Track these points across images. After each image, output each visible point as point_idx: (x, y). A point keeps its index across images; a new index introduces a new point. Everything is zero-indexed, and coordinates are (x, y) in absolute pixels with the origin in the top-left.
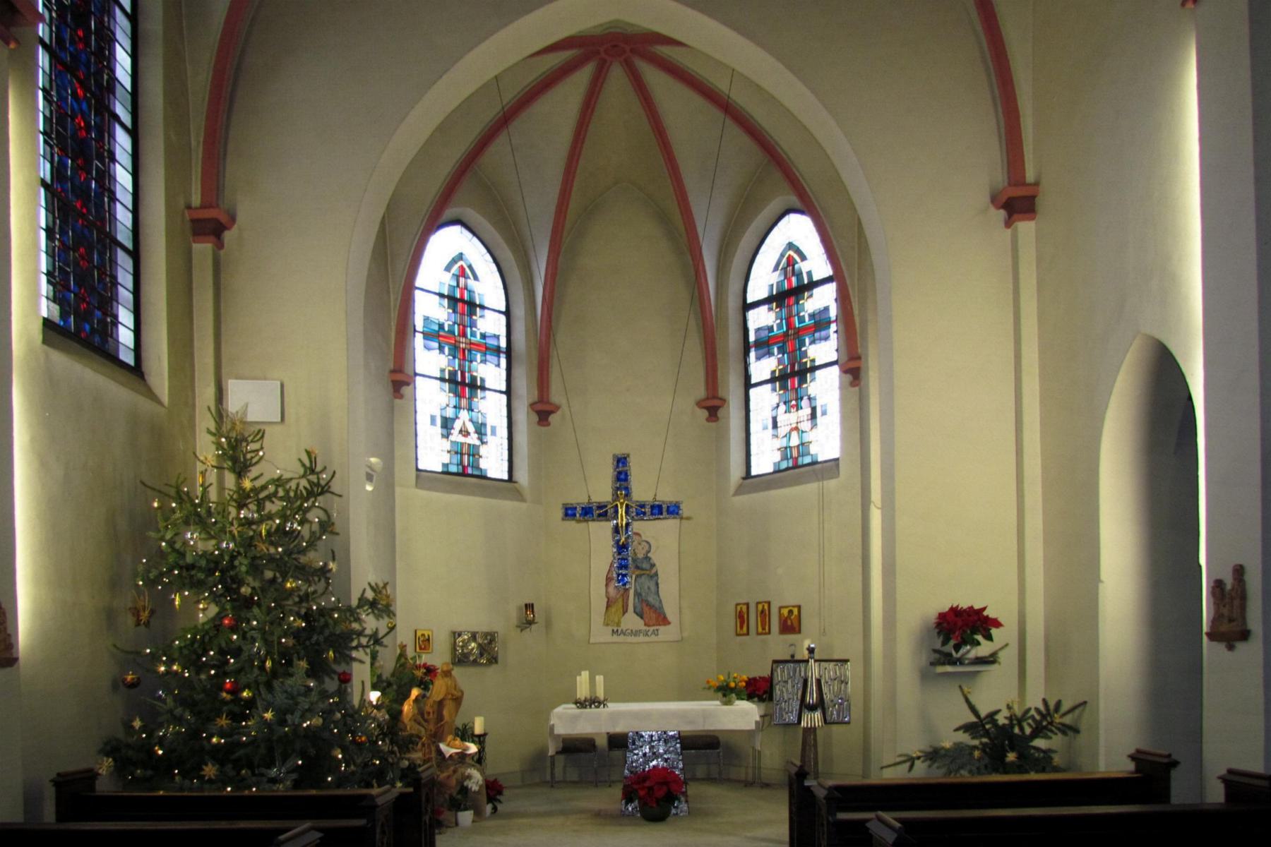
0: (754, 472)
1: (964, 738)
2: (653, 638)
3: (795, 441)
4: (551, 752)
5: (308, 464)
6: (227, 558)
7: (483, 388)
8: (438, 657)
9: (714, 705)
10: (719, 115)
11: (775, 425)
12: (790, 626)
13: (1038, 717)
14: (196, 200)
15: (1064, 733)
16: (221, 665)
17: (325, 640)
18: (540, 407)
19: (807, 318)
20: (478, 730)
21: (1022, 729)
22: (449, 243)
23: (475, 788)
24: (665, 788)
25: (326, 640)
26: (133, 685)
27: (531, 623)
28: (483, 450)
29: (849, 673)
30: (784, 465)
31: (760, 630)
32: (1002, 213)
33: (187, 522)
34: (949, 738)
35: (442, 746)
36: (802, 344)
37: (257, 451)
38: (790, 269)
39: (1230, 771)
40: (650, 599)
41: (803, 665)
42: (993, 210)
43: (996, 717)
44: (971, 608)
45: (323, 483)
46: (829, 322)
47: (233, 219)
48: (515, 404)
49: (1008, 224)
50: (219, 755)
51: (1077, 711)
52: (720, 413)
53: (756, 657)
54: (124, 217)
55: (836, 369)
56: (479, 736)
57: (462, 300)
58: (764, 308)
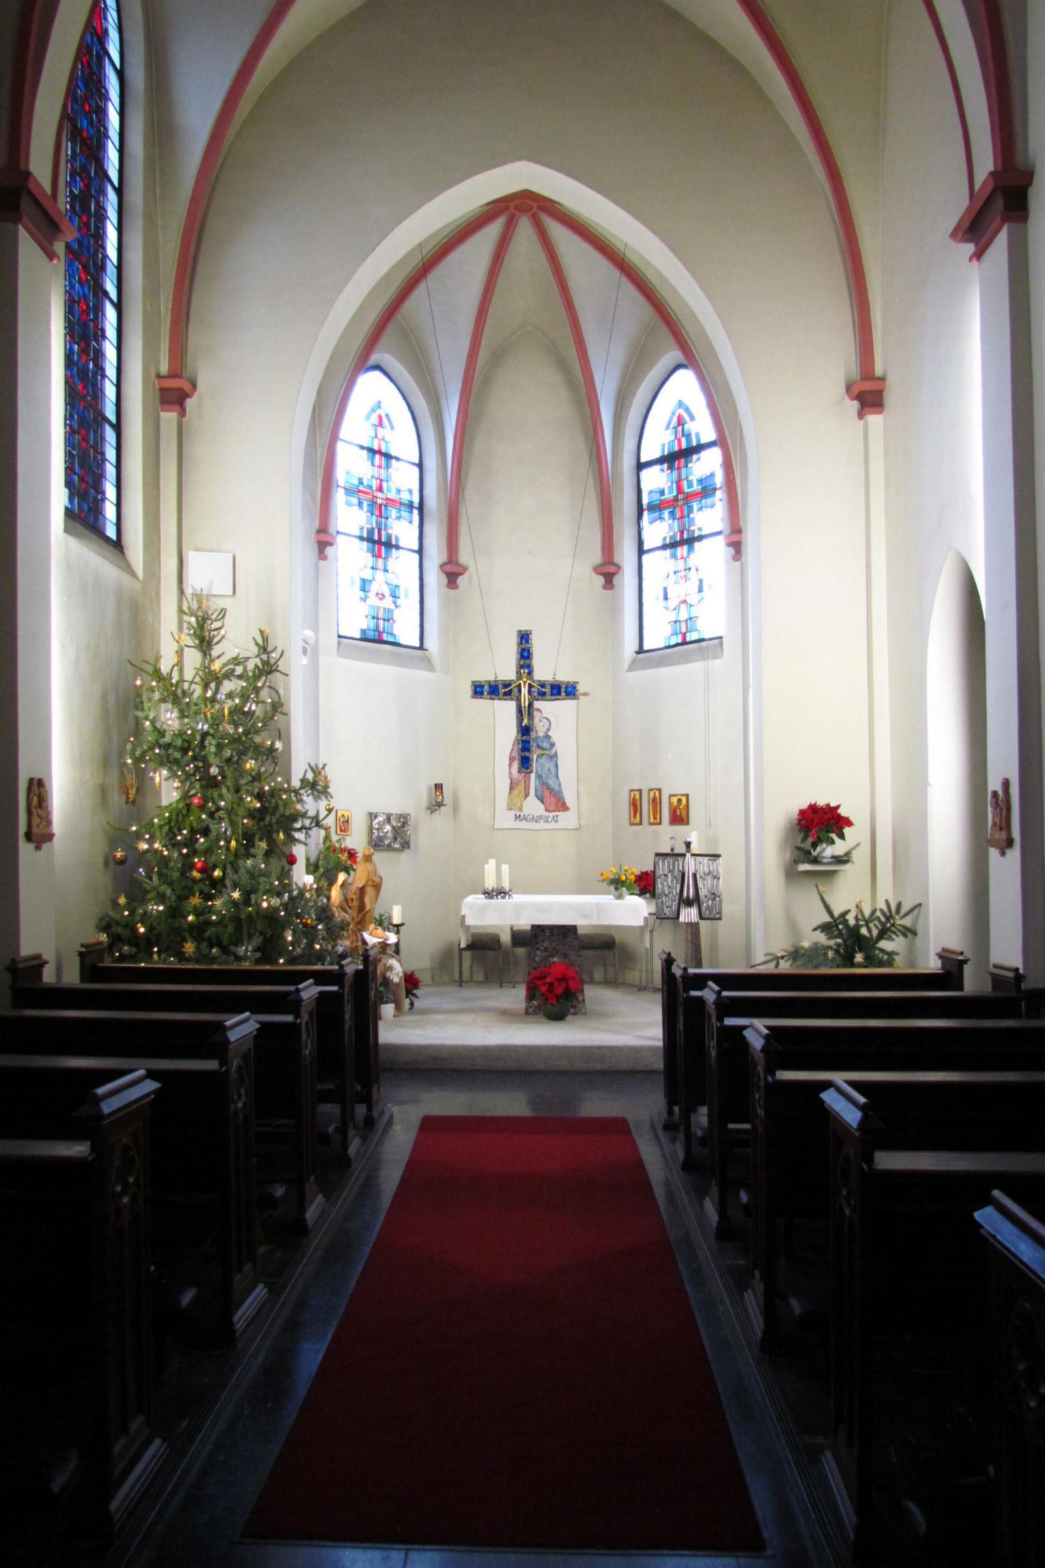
0: (646, 648)
1: (821, 938)
2: (553, 825)
3: (683, 616)
4: (463, 945)
5: (260, 642)
6: (198, 738)
7: (397, 547)
8: (357, 841)
9: (607, 899)
10: (615, 273)
11: (666, 598)
12: (679, 817)
13: (883, 919)
14: (164, 368)
15: (905, 936)
16: (190, 842)
17: (274, 820)
18: (449, 568)
19: (695, 483)
20: (396, 920)
21: (869, 931)
22: (372, 389)
23: (396, 980)
24: (564, 984)
25: (278, 822)
26: (122, 862)
27: (440, 804)
28: (397, 615)
29: (720, 869)
30: (673, 641)
31: (652, 820)
32: (856, 404)
33: (163, 700)
34: (811, 938)
35: (366, 935)
36: (690, 510)
37: (219, 629)
38: (680, 428)
39: (944, 950)
40: (550, 782)
41: (681, 859)
42: (847, 401)
43: (848, 917)
44: (828, 805)
45: (272, 662)
46: (715, 489)
47: (194, 386)
48: (426, 564)
49: (861, 415)
50: (197, 931)
51: (916, 911)
52: (616, 580)
53: (643, 848)
54: (110, 391)
55: (721, 538)
56: (397, 926)
57: (379, 452)
58: (657, 468)
